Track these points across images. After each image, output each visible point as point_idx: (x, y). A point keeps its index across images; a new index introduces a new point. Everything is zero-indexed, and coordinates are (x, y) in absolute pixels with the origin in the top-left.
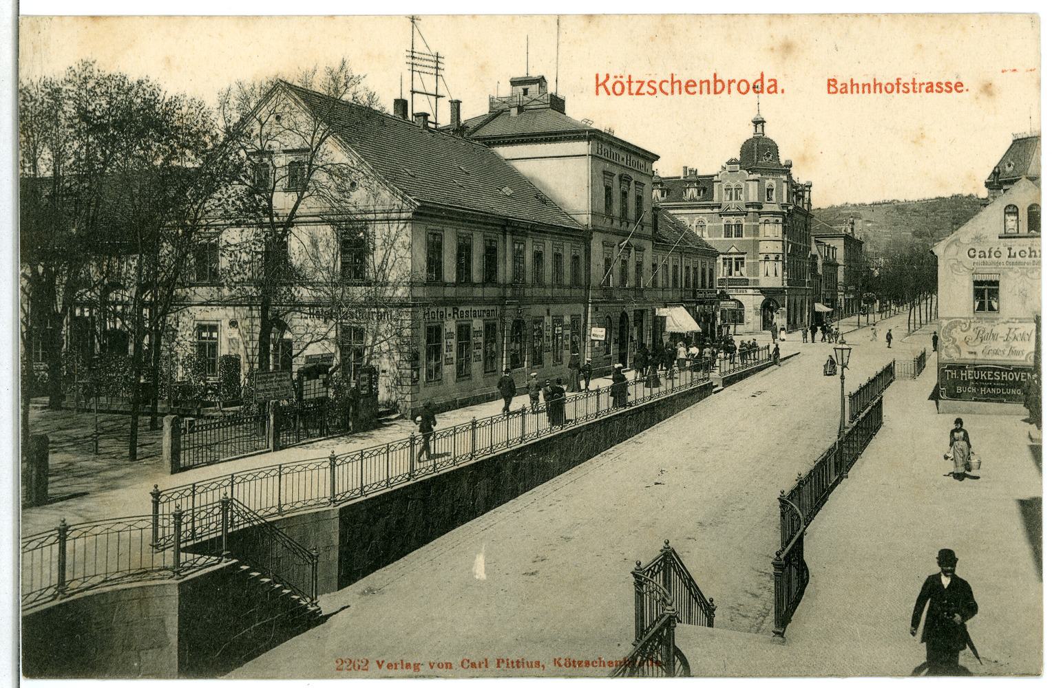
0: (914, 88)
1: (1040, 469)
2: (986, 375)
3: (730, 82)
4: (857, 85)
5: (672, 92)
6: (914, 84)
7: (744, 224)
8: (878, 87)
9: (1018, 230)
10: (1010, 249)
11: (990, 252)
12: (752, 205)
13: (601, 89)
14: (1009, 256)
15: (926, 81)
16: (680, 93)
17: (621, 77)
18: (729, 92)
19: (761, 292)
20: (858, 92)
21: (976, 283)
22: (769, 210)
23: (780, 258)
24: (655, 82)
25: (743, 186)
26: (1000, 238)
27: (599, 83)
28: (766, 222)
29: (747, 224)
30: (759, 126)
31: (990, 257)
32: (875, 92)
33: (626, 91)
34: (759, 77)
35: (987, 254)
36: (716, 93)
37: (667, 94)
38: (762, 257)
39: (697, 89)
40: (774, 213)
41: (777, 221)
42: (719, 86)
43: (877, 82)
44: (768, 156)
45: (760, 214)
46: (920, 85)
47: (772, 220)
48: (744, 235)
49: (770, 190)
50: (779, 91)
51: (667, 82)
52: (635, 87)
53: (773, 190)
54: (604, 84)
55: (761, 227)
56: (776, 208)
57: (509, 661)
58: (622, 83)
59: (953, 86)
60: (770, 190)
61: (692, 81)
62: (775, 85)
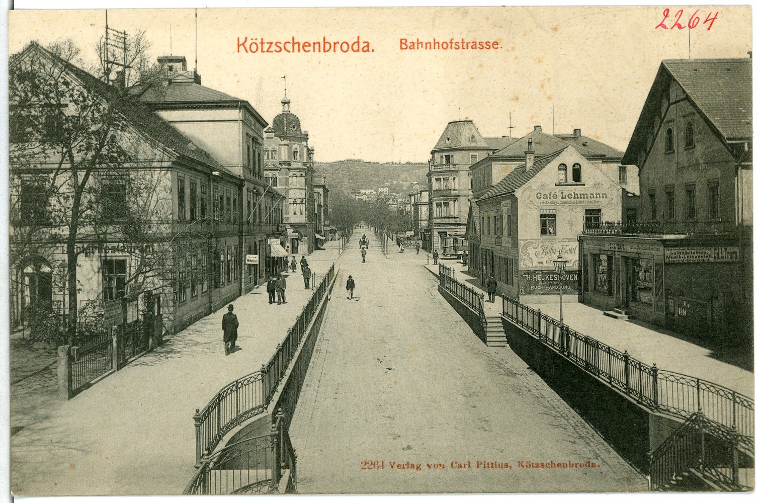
0: (463, 46)
2: (549, 277)
3: (335, 44)
4: (438, 43)
6: (463, 42)
7: (278, 177)
8: (437, 45)
9: (566, 179)
10: (562, 193)
11: (550, 195)
12: (285, 163)
13: (242, 48)
14: (562, 198)
15: (471, 40)
18: (334, 51)
19: (291, 226)
20: (430, 48)
21: (542, 216)
23: (304, 202)
24: (280, 43)
26: (556, 185)
27: (240, 44)
28: (295, 176)
29: (280, 177)
31: (550, 198)
32: (434, 48)
33: (332, 49)
35: (548, 196)
36: (325, 51)
37: (289, 52)
39: (311, 48)
41: (302, 175)
42: (327, 46)
43: (296, 41)
46: (467, 43)
47: (298, 174)
48: (278, 185)
49: (295, 152)
50: (370, 49)
51: (289, 43)
52: (266, 47)
54: (243, 44)
56: (300, 165)
57: (486, 463)
59: (491, 45)
60: (295, 152)
61: (306, 42)
62: (368, 46)
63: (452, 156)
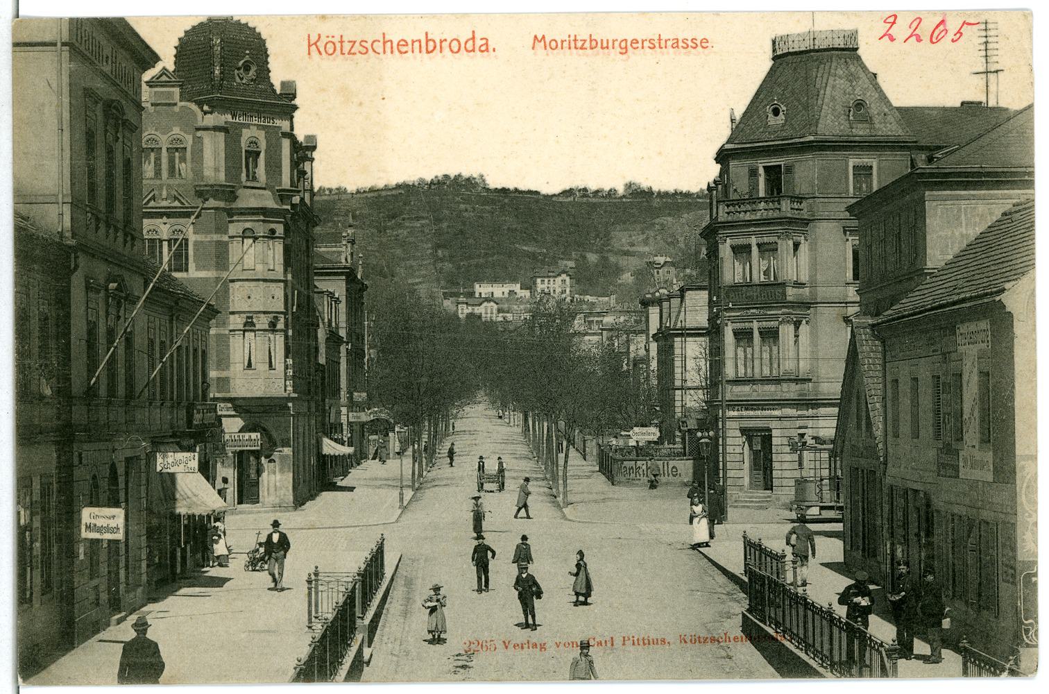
5: (384, 52)
6: (660, 40)
7: (192, 238)
16: (392, 52)
17: (333, 37)
22: (254, 203)
23: (280, 326)
24: (366, 42)
25: (189, 140)
28: (247, 234)
29: (199, 238)
34: (471, 36)
38: (237, 322)
40: (264, 211)
41: (273, 231)
42: (431, 44)
44: (247, 68)
45: (230, 213)
47: (261, 230)
48: (192, 265)
50: (491, 49)
53: (258, 154)
54: (315, 44)
55: (235, 249)
58: (334, 44)
59: (698, 43)
60: (253, 155)
62: (487, 44)
63: (789, 169)
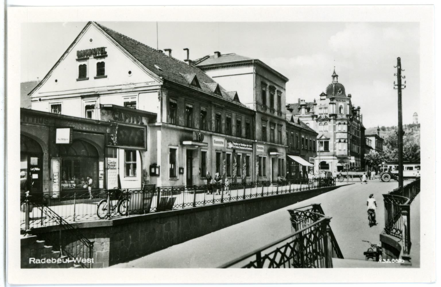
1: (242, 268)
23: (347, 141)
28: (340, 124)
30: (336, 78)
38: (338, 141)
